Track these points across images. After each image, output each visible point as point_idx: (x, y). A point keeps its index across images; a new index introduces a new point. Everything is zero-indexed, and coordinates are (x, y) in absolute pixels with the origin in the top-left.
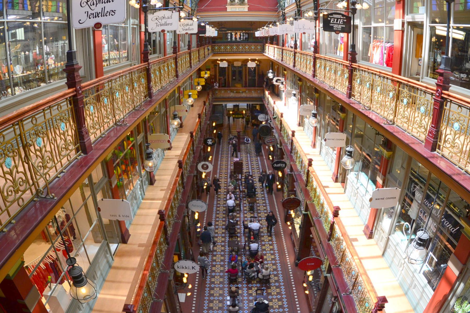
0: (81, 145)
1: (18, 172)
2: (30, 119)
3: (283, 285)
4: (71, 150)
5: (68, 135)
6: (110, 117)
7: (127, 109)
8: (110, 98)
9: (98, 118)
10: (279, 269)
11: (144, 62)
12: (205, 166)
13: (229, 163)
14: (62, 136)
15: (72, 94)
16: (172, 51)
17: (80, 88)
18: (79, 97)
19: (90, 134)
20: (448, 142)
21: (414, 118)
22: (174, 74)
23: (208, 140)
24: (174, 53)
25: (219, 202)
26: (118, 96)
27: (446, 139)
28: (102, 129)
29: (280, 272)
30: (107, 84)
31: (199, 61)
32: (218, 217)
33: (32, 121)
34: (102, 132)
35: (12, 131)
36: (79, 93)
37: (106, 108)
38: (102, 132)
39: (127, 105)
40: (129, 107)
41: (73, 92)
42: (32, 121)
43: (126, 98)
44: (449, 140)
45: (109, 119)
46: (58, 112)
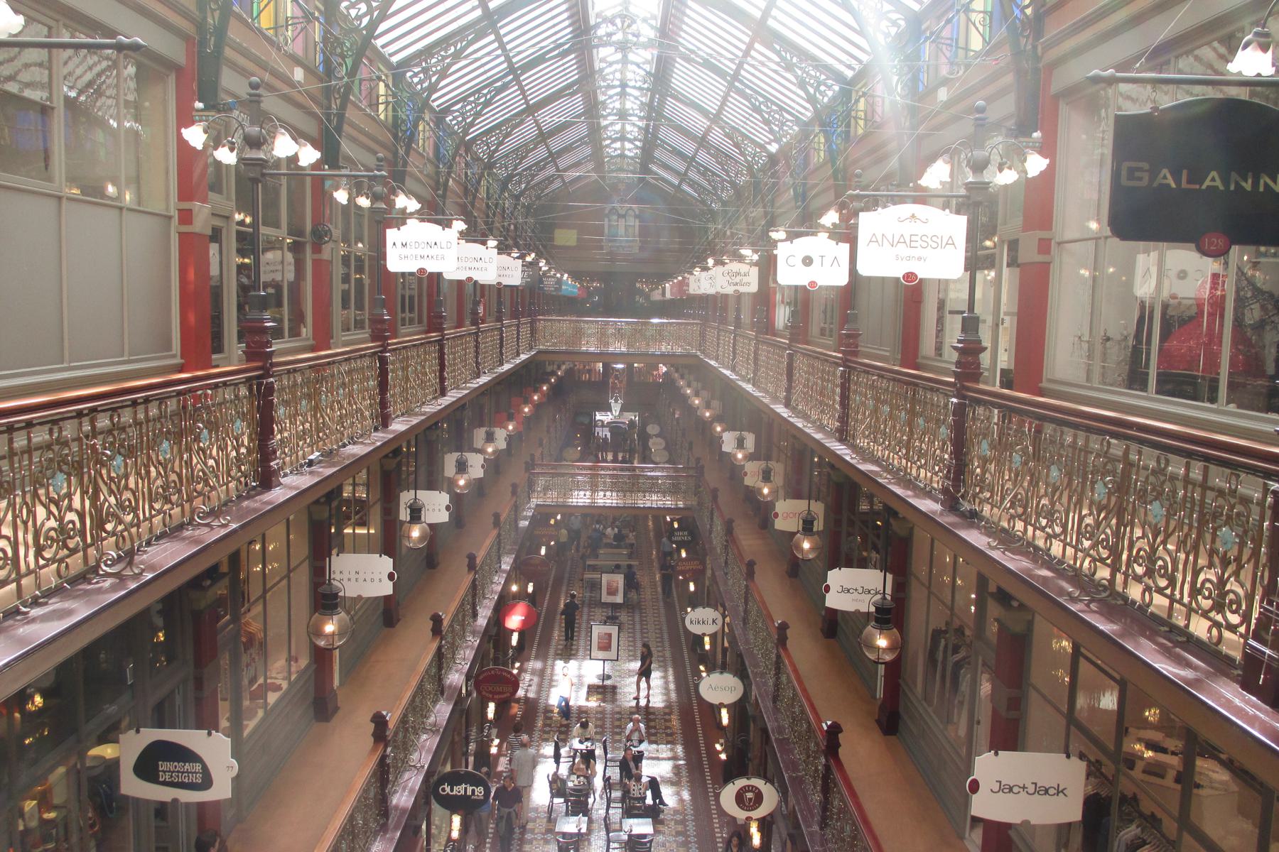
1: (70, 508)
3: (695, 842)
12: (750, 795)
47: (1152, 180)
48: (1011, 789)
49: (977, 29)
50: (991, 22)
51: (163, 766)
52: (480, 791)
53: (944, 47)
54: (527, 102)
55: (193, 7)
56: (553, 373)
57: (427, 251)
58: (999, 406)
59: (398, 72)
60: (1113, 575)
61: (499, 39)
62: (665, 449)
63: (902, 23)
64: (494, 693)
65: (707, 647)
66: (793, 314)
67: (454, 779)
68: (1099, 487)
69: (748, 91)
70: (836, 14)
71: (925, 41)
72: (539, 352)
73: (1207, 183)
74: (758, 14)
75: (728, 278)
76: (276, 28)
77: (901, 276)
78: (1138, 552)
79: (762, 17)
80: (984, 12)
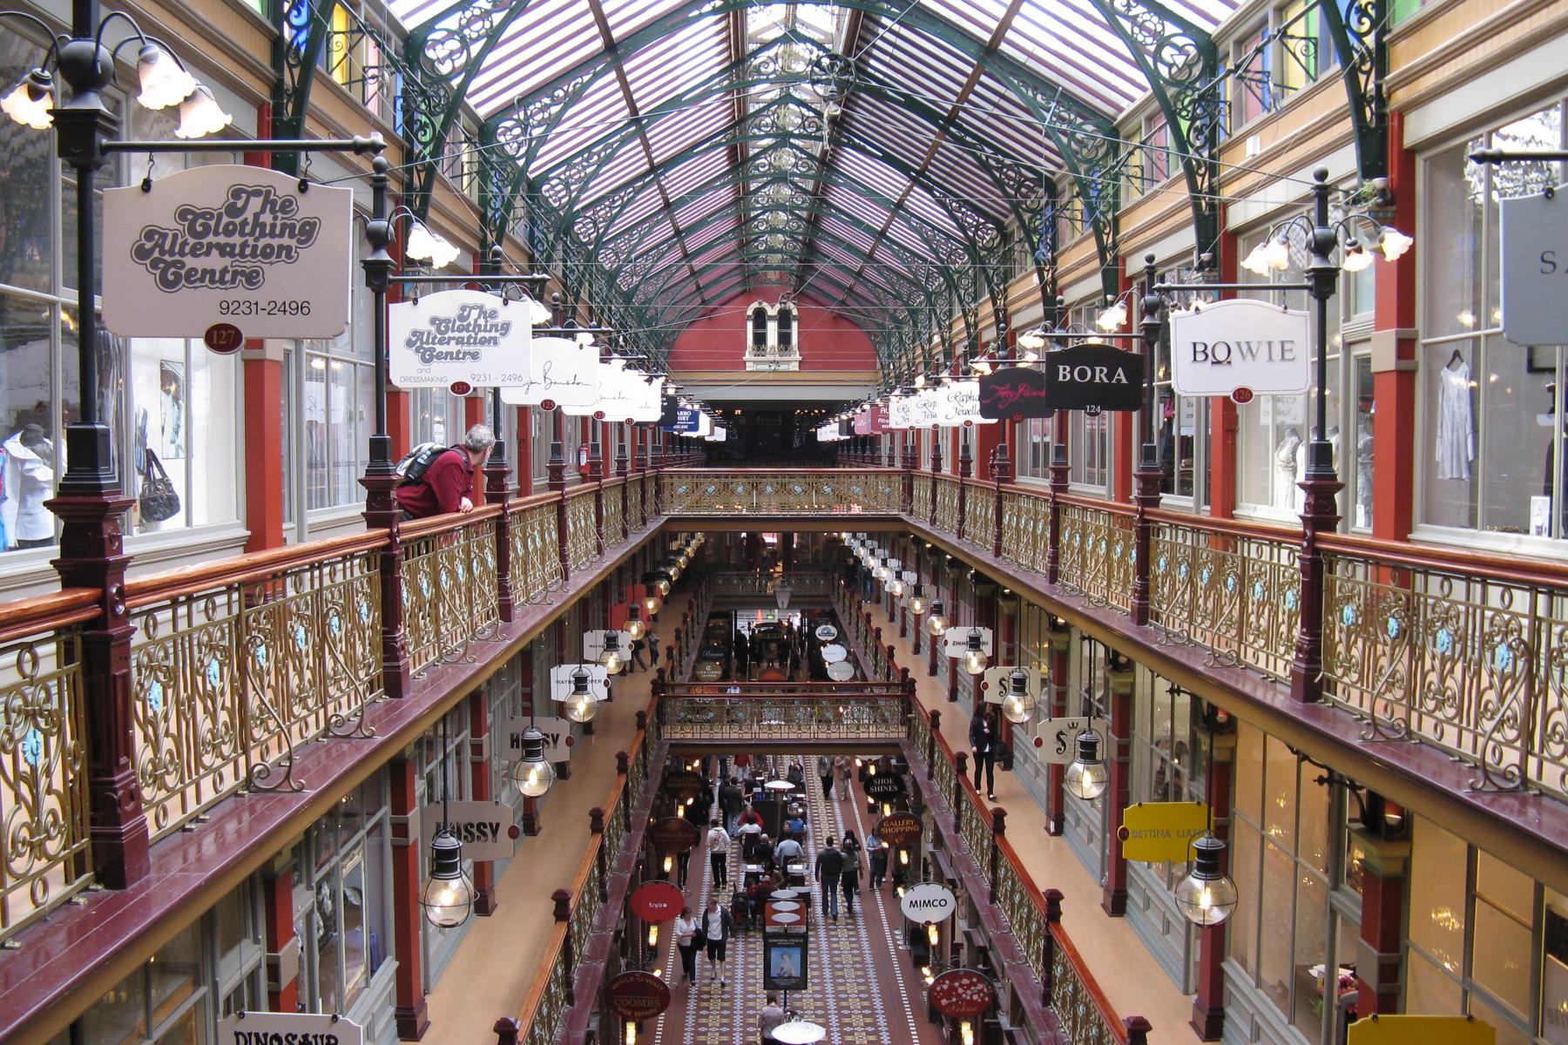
0: (94, 846)
4: (53, 860)
5: (49, 791)
6: (311, 702)
7: (207, 784)
8: (176, 687)
11: (489, 502)
14: (24, 789)
15: (85, 615)
16: (361, 507)
17: (121, 591)
19: (10, 882)
20: (1557, 738)
22: (370, 664)
23: (778, 894)
24: (372, 520)
28: (191, 792)
30: (168, 614)
31: (600, 549)
34: (190, 810)
36: (116, 615)
37: (214, 703)
38: (190, 810)
39: (297, 710)
40: (305, 718)
41: (381, 537)
45: (163, 786)
46: (17, 678)
49: (1298, 60)
50: (1316, 51)
53: (1253, 84)
54: (651, 161)
55: (63, 12)
56: (680, 552)
58: (1366, 560)
59: (485, 132)
60: (1524, 760)
61: (622, 77)
62: (846, 660)
63: (1192, 51)
64: (634, 1009)
68: (1501, 651)
69: (968, 139)
70: (1070, 20)
71: (1227, 75)
72: (671, 520)
74: (987, 37)
75: (955, 404)
76: (350, 83)
77: (1231, 394)
78: (1486, 705)
79: (992, 40)
80: (1307, 38)
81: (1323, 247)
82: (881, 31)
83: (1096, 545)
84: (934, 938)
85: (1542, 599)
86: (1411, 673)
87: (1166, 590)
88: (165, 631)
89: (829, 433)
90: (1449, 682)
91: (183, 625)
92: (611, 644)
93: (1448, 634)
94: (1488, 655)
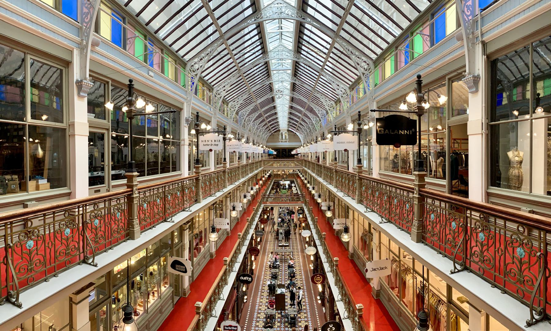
2: (63, 213)
9: (150, 214)
10: (309, 317)
13: (276, 245)
18: (134, 196)
20: (476, 256)
21: (446, 236)
25: (263, 288)
26: (179, 195)
27: (473, 252)
29: (309, 319)
32: (263, 296)
33: (117, 201)
35: (3, 229)
42: (117, 201)
43: (192, 195)
44: (476, 253)
47: (384, 132)
48: (375, 270)
51: (177, 266)
52: (250, 279)
57: (236, 147)
65: (150, 108)
66: (526, 88)
67: (244, 276)
73: (395, 132)
78: (475, 252)
81: (359, 125)
82: (298, 75)
83: (345, 181)
84: (306, 245)
85: (542, 233)
86: (390, 208)
87: (365, 195)
88: (171, 188)
89: (293, 152)
90: (397, 211)
91: (174, 187)
92: (252, 189)
93: (434, 216)
94: (405, 206)
